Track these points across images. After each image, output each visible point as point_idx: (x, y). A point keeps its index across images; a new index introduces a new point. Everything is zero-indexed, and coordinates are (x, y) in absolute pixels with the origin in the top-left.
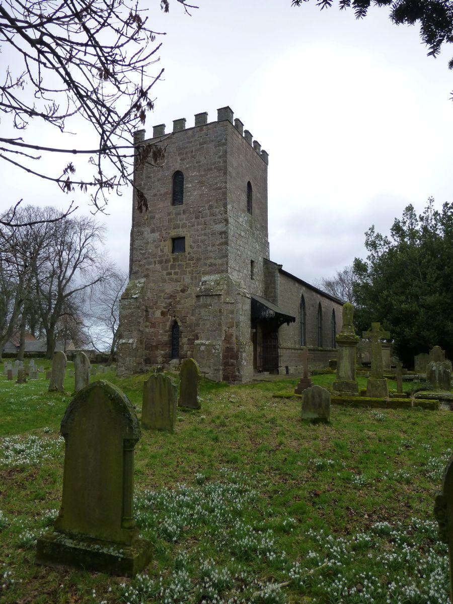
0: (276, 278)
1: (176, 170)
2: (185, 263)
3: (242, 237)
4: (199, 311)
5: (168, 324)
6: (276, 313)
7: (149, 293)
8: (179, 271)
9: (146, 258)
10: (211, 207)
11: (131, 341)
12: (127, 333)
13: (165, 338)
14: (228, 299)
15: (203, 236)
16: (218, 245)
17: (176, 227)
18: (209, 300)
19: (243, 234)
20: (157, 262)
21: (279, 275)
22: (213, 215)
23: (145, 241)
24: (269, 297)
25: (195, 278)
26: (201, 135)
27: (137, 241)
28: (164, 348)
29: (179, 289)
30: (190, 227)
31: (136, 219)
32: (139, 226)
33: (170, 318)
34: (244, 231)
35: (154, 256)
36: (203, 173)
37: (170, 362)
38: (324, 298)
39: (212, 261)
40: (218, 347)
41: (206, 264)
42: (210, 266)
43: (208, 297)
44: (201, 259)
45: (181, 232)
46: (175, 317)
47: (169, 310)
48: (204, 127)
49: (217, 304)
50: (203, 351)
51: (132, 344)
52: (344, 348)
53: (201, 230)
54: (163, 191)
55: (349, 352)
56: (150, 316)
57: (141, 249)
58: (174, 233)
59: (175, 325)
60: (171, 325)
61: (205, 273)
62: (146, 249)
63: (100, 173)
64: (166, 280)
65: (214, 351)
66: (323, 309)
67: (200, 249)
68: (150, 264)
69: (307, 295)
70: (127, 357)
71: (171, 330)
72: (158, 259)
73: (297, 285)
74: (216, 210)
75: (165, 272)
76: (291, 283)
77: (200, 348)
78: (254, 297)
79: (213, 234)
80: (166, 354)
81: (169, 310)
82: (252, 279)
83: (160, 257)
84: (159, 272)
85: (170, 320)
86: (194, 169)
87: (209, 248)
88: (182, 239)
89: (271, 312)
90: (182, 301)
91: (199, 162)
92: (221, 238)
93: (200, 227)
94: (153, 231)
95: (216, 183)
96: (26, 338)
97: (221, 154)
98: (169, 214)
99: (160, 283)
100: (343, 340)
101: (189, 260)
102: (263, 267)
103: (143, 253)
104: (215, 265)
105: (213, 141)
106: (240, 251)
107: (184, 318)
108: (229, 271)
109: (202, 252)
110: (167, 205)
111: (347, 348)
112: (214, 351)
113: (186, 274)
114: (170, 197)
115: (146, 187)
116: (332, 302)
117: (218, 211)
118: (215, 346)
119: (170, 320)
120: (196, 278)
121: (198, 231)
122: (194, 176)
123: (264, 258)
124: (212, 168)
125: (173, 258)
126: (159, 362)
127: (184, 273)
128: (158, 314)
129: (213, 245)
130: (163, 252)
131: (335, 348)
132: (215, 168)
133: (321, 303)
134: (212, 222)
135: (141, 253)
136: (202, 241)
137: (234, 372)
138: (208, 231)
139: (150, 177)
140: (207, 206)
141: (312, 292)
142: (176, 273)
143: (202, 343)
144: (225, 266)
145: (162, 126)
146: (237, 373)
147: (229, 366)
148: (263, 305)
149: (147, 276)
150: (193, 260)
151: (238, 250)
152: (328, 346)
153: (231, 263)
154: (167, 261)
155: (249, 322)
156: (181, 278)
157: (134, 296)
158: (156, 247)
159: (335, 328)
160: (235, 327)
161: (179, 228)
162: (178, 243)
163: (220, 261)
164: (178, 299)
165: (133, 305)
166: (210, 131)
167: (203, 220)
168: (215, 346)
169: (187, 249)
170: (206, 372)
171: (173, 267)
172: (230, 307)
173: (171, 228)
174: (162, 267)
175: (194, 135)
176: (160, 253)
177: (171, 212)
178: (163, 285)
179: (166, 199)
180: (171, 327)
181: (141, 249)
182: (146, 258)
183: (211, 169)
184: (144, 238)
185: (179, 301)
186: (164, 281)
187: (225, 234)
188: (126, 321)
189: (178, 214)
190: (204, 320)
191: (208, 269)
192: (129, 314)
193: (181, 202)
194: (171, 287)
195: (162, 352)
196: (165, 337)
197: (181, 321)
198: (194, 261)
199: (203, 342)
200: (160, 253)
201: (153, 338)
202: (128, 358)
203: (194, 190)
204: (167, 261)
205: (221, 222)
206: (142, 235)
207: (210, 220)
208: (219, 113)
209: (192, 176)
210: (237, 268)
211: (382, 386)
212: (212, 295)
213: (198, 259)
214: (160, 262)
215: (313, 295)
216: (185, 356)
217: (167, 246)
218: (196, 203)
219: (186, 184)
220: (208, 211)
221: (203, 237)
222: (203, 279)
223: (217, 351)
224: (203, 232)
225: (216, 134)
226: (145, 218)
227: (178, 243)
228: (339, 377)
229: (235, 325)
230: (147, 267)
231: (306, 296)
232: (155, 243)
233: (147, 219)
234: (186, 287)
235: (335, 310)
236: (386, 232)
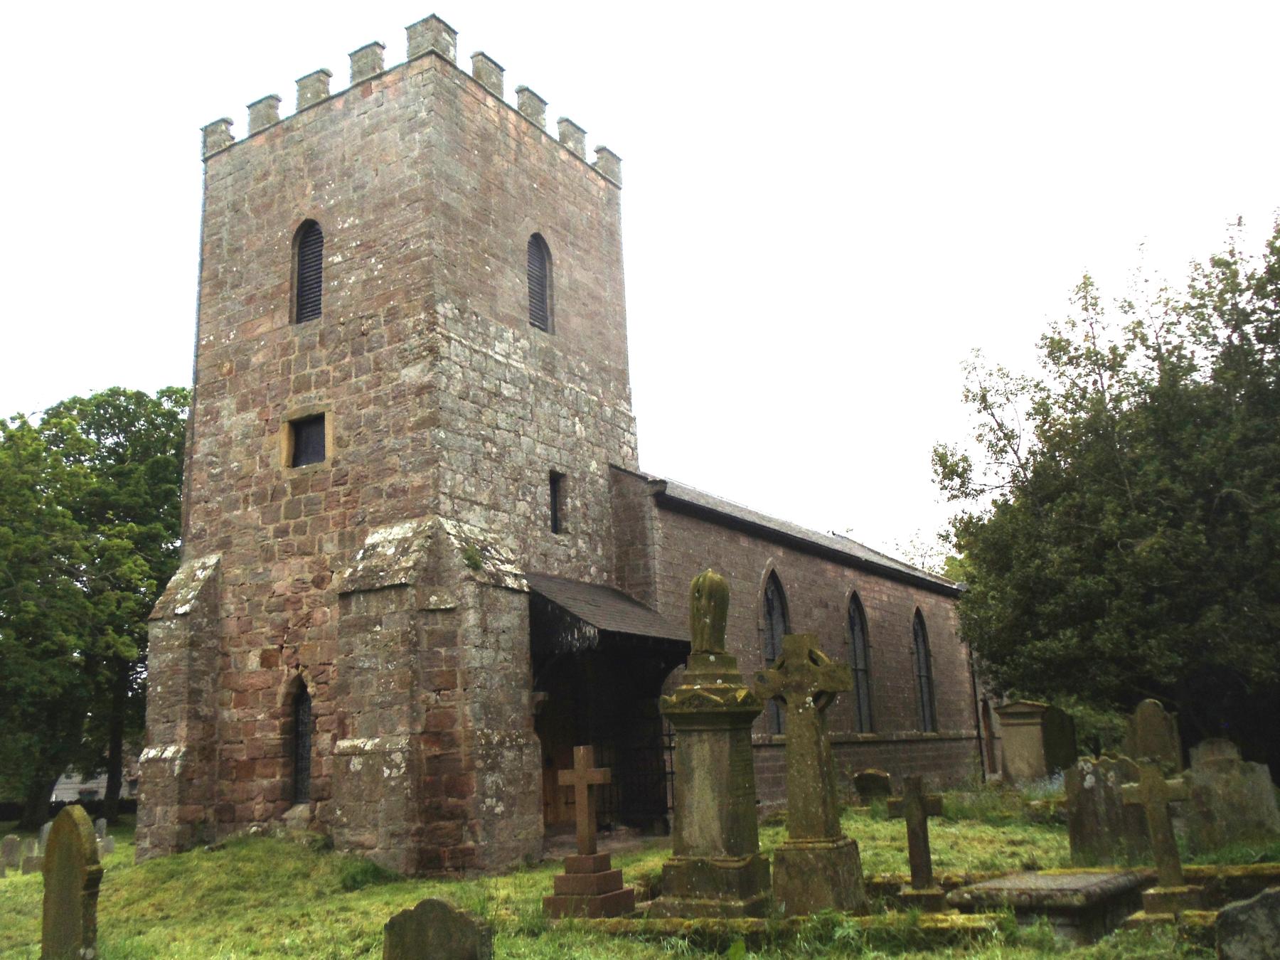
0: (648, 524)
1: (303, 218)
2: (323, 494)
3: (506, 399)
4: (349, 644)
5: (282, 689)
6: (602, 632)
7: (230, 595)
8: (308, 520)
9: (223, 491)
10: (392, 315)
11: (170, 752)
12: (162, 727)
13: (274, 737)
14: (433, 599)
15: (371, 407)
16: (411, 429)
17: (302, 385)
18: (373, 606)
19: (507, 390)
20: (251, 499)
21: (655, 512)
22: (398, 337)
23: (220, 438)
24: (630, 585)
25: (351, 540)
26: (367, 107)
27: (203, 441)
28: (269, 771)
29: (309, 577)
30: (338, 382)
31: (201, 375)
32: (210, 395)
33: (286, 671)
34: (513, 382)
35: (243, 478)
36: (372, 217)
37: (285, 816)
38: (873, 579)
39: (395, 479)
40: (398, 757)
41: (378, 492)
42: (389, 496)
43: (372, 597)
44: (366, 477)
45: (316, 400)
46: (297, 667)
47: (282, 647)
48: (374, 83)
49: (397, 616)
50: (358, 773)
51: (173, 760)
52: (695, 738)
53: (369, 389)
54: (270, 283)
55: (712, 751)
56: (233, 670)
57: (211, 464)
58: (295, 406)
59: (298, 696)
60: (287, 695)
61: (378, 522)
62: (224, 463)
63: (993, 415)
64: (273, 555)
65: (387, 772)
66: (869, 612)
67: (363, 448)
68: (233, 505)
69: (794, 573)
70: (156, 805)
71: (288, 710)
72: (254, 489)
73: (744, 542)
74: (405, 321)
75: (271, 528)
76: (716, 539)
77: (348, 763)
78: (545, 589)
79: (399, 395)
80: (273, 788)
81: (282, 647)
82: (556, 529)
83: (260, 481)
84: (258, 529)
85: (285, 678)
86: (349, 207)
87: (389, 442)
88: (319, 419)
89: (590, 631)
90: (318, 615)
91: (363, 187)
92: (421, 405)
93: (364, 378)
94: (243, 407)
95: (406, 242)
96: (726, 747)
97: (416, 153)
98: (286, 349)
99: (259, 564)
100: (686, 710)
101: (336, 484)
102: (610, 492)
103: (217, 475)
104: (404, 491)
105: (394, 120)
106: (495, 444)
107: (322, 668)
108: (446, 505)
109: (368, 456)
110: (279, 324)
111: (705, 736)
112: (387, 772)
113: (325, 530)
114: (286, 299)
115: (229, 280)
116: (912, 591)
117: (410, 325)
118: (390, 753)
119: (285, 678)
120: (352, 537)
121: (359, 390)
122: (348, 228)
123: (612, 466)
124: (394, 198)
125: (293, 482)
126: (257, 814)
127: (321, 523)
128: (253, 661)
129: (399, 431)
130: (267, 465)
131: (934, 730)
132: (401, 197)
133: (862, 594)
134: (395, 359)
135: (211, 476)
136: (372, 421)
137: (460, 840)
138: (386, 388)
139: (238, 250)
140: (382, 313)
141: (819, 561)
142: (300, 530)
143: (355, 747)
144: (431, 492)
145: (273, 100)
146: (471, 844)
147: (443, 818)
148: (563, 611)
149: (225, 545)
150: (345, 483)
151: (485, 439)
152: (902, 727)
153: (454, 480)
154: (277, 494)
155: (524, 669)
156: (312, 542)
157: (180, 611)
158: (250, 454)
159: (928, 669)
160: (459, 690)
161: (308, 389)
162: (306, 434)
163: (417, 479)
164: (305, 609)
165: (178, 638)
166: (390, 93)
167: (371, 356)
168: (390, 753)
169: (330, 450)
170: (367, 843)
171: (293, 511)
172: (441, 624)
173: (288, 391)
174: (263, 514)
175: (350, 110)
176: (259, 471)
177: (290, 343)
178: (265, 569)
179: (277, 307)
180: (289, 702)
181: (211, 464)
182: (223, 491)
183: (391, 204)
184: (220, 429)
185: (308, 617)
186: (268, 556)
187: (430, 393)
188: (159, 689)
189: (307, 348)
190: (363, 671)
191: (384, 505)
192: (167, 666)
193: (316, 312)
194: (287, 572)
195: (265, 782)
196: (271, 735)
197: (314, 677)
198: (348, 486)
199: (359, 742)
200: (259, 471)
201: (241, 738)
202: (159, 808)
203: (349, 271)
204: (277, 494)
205: (419, 357)
206: (215, 419)
207: (391, 353)
208: (410, 38)
209: (342, 230)
210: (484, 498)
211: (825, 868)
212: (383, 589)
213: (360, 479)
214: (260, 498)
215: (822, 573)
216: (326, 794)
217: (281, 444)
218: (353, 309)
219: (328, 257)
220: (383, 329)
221: (371, 409)
222: (369, 540)
223: (395, 773)
224: (372, 394)
225: (403, 99)
226: (225, 370)
227: (306, 434)
228: (681, 849)
229: (458, 682)
230: (226, 515)
231: (785, 574)
232: (249, 441)
233: (230, 372)
234: (325, 568)
235: (925, 614)
236: (1031, 364)
